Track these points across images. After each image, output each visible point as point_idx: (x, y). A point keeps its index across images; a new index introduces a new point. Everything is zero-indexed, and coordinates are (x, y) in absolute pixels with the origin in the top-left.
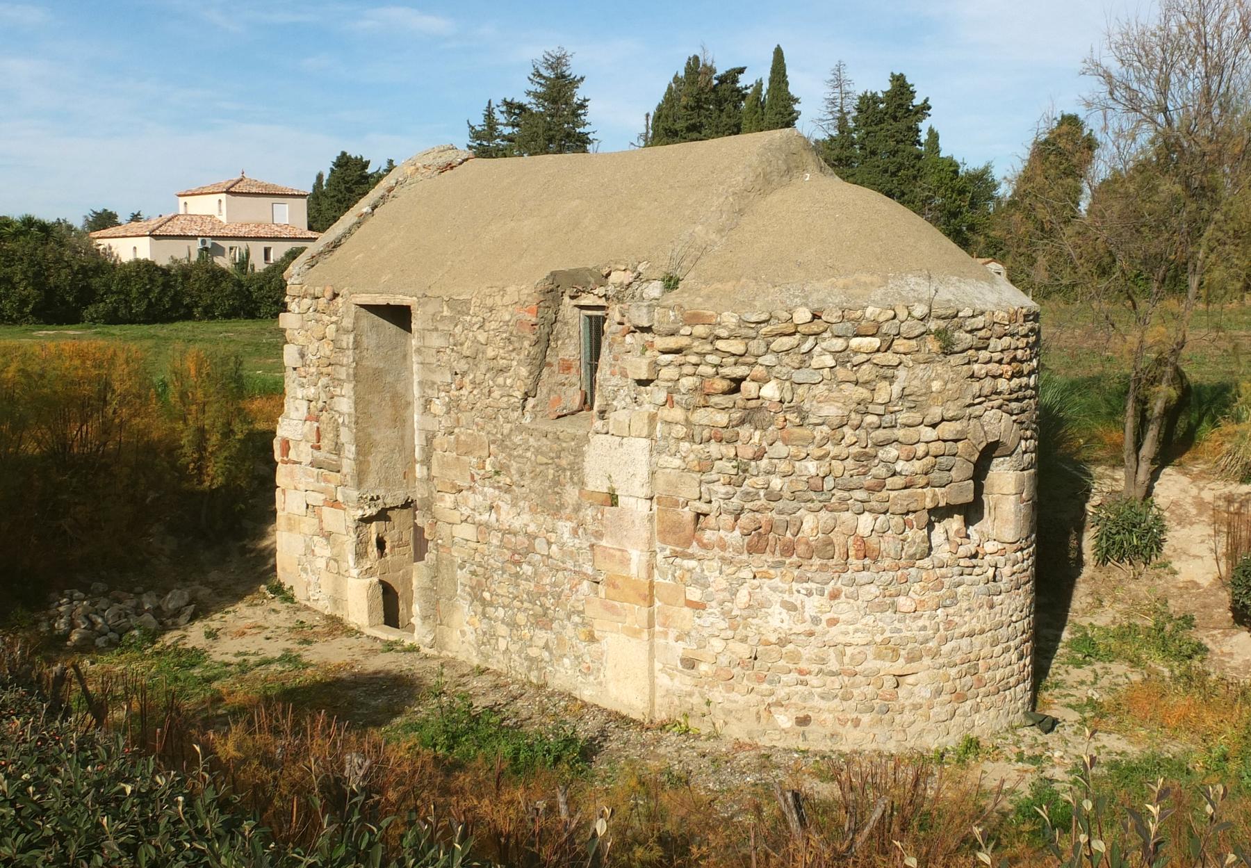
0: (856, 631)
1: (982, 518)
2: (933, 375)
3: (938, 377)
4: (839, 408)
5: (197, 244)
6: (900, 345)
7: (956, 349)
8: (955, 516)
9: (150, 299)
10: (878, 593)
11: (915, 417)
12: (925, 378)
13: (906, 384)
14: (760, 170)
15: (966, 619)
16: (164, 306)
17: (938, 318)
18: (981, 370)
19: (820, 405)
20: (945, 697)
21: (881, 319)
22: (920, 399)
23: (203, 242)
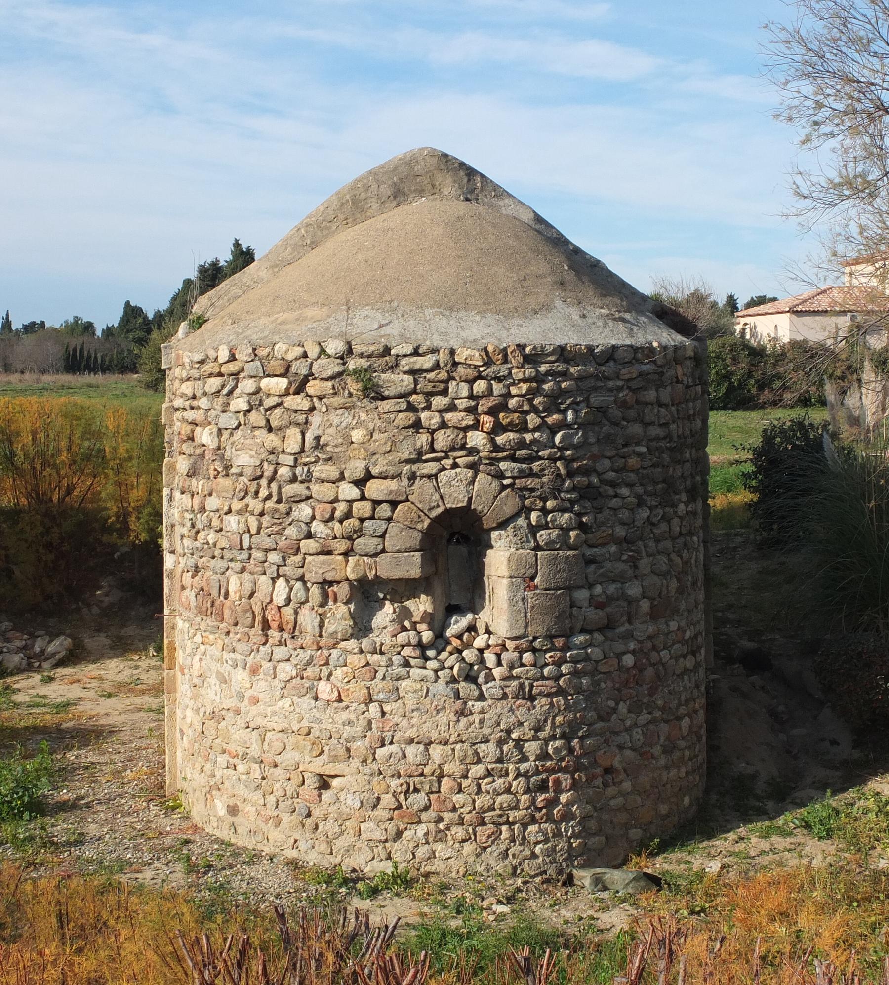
0: (274, 713)
1: (483, 608)
2: (354, 422)
3: (360, 424)
4: (251, 457)
5: (845, 321)
6: (313, 387)
7: (386, 393)
8: (423, 596)
9: (731, 383)
10: (294, 673)
11: (331, 471)
12: (343, 425)
13: (320, 432)
14: (348, 197)
15: (414, 721)
16: (749, 391)
17: (361, 356)
18: (431, 418)
19: (238, 453)
20: (381, 813)
21: (290, 357)
22: (336, 450)
23: (853, 318)
